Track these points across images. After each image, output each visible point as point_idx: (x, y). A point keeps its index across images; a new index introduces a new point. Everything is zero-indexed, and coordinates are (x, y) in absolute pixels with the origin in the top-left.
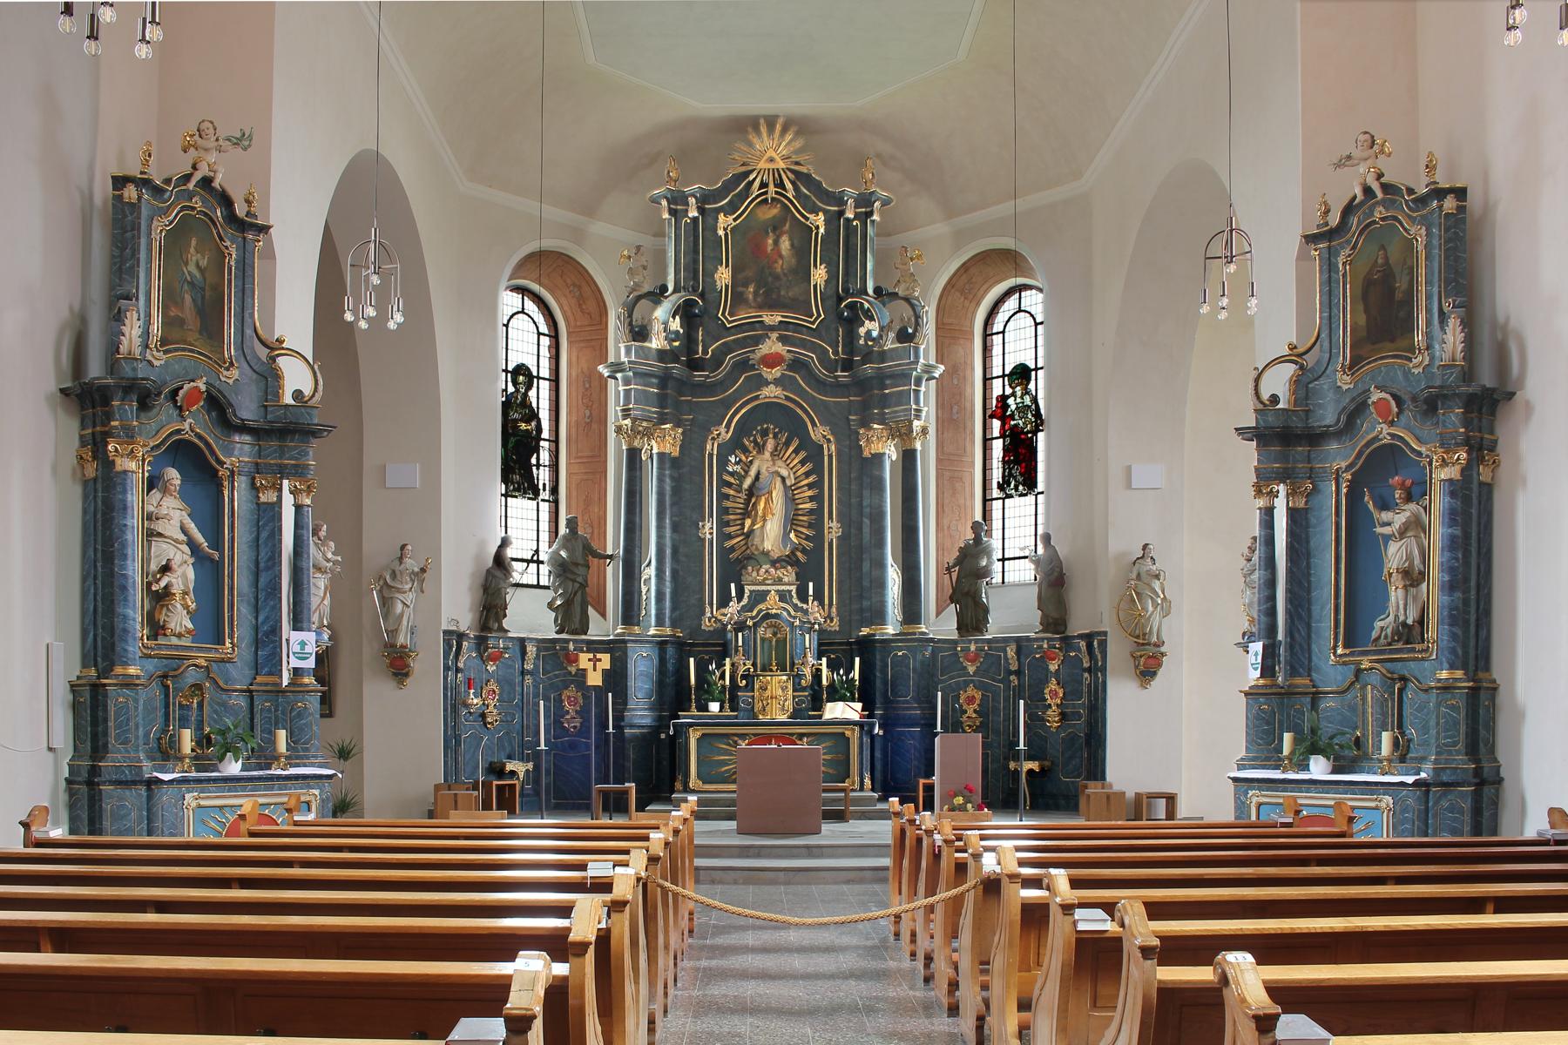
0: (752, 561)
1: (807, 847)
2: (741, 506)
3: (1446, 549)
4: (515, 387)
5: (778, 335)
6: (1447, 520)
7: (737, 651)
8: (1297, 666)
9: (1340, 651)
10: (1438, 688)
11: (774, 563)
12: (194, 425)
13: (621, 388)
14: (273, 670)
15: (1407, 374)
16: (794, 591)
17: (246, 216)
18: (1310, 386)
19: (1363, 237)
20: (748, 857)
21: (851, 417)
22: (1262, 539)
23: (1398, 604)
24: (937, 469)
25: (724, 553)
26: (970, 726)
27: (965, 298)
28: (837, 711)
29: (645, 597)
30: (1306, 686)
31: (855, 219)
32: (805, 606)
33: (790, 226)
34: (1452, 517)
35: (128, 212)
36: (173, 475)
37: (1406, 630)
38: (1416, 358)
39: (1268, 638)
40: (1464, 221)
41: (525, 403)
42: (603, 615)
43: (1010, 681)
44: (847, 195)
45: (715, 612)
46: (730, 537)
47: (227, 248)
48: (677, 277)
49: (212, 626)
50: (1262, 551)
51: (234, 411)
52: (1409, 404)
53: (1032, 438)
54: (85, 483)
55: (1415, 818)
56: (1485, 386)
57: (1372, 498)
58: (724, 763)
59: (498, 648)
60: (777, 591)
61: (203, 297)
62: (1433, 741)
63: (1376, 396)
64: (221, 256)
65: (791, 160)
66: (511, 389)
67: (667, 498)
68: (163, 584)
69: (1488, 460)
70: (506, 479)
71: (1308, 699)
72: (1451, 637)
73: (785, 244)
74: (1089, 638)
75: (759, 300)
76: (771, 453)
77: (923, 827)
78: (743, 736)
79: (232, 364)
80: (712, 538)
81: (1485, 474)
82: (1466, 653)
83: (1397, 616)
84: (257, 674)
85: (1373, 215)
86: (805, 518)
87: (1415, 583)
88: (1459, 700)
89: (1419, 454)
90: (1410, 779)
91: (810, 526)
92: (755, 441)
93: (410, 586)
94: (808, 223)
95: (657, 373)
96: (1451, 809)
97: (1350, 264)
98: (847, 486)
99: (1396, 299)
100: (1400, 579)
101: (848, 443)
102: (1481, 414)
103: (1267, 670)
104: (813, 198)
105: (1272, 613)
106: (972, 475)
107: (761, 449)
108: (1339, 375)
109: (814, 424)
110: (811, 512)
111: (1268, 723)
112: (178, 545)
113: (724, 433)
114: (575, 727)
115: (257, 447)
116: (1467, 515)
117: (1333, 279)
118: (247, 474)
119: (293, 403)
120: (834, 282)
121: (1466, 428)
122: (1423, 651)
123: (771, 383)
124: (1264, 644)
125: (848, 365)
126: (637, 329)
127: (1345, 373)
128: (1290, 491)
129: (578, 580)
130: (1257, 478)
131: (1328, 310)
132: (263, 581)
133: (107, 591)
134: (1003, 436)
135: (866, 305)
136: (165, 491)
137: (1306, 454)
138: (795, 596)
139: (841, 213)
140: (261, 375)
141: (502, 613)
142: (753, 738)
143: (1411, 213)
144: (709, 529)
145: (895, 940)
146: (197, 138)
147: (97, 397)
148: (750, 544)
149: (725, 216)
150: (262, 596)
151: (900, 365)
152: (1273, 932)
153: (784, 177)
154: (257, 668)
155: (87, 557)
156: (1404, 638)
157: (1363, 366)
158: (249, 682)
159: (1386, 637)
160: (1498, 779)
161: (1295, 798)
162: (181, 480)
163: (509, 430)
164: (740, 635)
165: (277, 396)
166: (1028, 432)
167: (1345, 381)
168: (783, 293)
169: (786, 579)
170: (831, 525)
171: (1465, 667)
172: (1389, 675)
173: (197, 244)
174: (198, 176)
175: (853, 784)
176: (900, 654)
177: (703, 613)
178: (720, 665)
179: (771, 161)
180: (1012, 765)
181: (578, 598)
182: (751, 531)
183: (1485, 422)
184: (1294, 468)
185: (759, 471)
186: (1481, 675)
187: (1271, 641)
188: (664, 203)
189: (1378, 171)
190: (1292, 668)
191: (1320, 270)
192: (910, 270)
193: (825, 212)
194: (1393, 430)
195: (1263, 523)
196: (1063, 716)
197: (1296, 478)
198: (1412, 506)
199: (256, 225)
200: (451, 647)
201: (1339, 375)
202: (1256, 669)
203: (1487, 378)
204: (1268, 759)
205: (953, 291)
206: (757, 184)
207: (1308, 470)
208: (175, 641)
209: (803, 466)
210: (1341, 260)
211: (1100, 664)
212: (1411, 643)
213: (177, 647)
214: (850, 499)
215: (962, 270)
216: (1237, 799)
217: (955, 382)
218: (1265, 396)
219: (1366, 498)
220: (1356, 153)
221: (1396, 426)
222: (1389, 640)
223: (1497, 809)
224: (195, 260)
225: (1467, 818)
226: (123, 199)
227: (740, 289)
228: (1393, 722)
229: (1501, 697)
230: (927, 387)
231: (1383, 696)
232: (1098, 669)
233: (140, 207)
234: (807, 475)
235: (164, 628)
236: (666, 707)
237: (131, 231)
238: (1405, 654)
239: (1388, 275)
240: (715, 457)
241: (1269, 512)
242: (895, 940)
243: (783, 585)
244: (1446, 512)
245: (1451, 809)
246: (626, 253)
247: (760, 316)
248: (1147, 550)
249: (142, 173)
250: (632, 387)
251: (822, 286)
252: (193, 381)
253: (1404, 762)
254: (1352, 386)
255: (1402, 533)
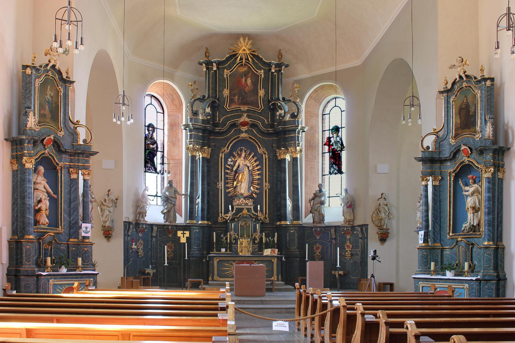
0: (237, 197)
1: (261, 301)
2: (232, 177)
3: (487, 201)
4: (149, 132)
5: (246, 115)
6: (487, 191)
7: (231, 230)
8: (436, 239)
9: (451, 234)
10: (484, 248)
11: (245, 198)
12: (49, 151)
13: (189, 133)
14: (76, 237)
15: (474, 140)
16: (252, 208)
17: (66, 78)
18: (441, 143)
19: (459, 93)
20: (240, 304)
21: (274, 145)
22: (424, 196)
23: (471, 219)
24: (305, 164)
25: (226, 194)
26: (318, 258)
27: (316, 102)
28: (267, 252)
29: (197, 210)
30: (439, 246)
31: (275, 72)
32: (256, 214)
33: (251, 75)
34: (489, 190)
35: (27, 77)
36: (41, 169)
37: (474, 228)
38: (477, 135)
39: (426, 230)
40: (493, 89)
41: (152, 138)
42: (181, 216)
43: (332, 242)
44: (272, 63)
45: (223, 215)
46: (228, 188)
47: (60, 89)
48: (209, 92)
49: (54, 222)
50: (424, 200)
51: (63, 147)
52: (474, 151)
53: (340, 153)
54: (13, 171)
55: (476, 291)
56: (500, 146)
57: (462, 182)
58: (227, 271)
59: (143, 228)
60: (246, 208)
61: (52, 107)
62: (482, 265)
63: (463, 147)
64: (58, 92)
65: (251, 50)
66: (147, 132)
67: (206, 174)
68: (39, 206)
69: (501, 171)
70: (145, 166)
71: (440, 251)
72: (488, 231)
73: (249, 81)
74: (361, 226)
75: (239, 101)
76: (244, 158)
77: (310, 293)
78: (234, 261)
79: (61, 130)
80: (222, 188)
81: (500, 175)
82: (493, 236)
83: (470, 223)
84: (70, 238)
85: (462, 85)
86: (256, 182)
87: (477, 211)
88: (491, 252)
89: (478, 168)
90: (474, 278)
91: (258, 184)
92: (238, 153)
93: (111, 205)
94: (257, 73)
95: (202, 128)
96: (488, 289)
97: (454, 102)
98: (272, 170)
99: (470, 114)
100: (471, 210)
101: (272, 154)
102: (499, 155)
103: (425, 241)
104: (259, 64)
105: (427, 221)
106: (318, 167)
107: (240, 156)
108: (450, 140)
109: (260, 147)
110: (259, 179)
111: (426, 259)
112: (43, 193)
113: (226, 150)
114: (171, 257)
115: (70, 159)
116: (494, 189)
117: (448, 107)
118: (67, 168)
119: (83, 144)
120: (267, 96)
121: (493, 160)
122: (479, 235)
123: (244, 132)
124: (424, 232)
125: (272, 126)
126: (194, 112)
127: (453, 139)
128: (433, 179)
129: (173, 203)
130: (422, 174)
131: (447, 117)
132: (72, 206)
133: (21, 209)
134: (329, 152)
135: (279, 104)
136: (38, 174)
137: (439, 166)
138: (253, 210)
139: (270, 70)
140: (72, 134)
141: (144, 215)
142: (238, 262)
143: (475, 85)
144: (221, 185)
145: (298, 331)
146: (50, 51)
147: (18, 142)
148: (236, 191)
149: (226, 70)
150: (72, 211)
151: (292, 127)
152: (423, 322)
153: (249, 56)
154: (70, 236)
155: (14, 197)
156: (473, 230)
157: (459, 137)
158: (67, 240)
159: (467, 230)
160: (505, 278)
161: (435, 285)
162: (44, 170)
163: (147, 148)
164: (233, 224)
165: (77, 141)
166: (338, 151)
167: (452, 141)
168: (248, 99)
169: (249, 204)
170: (266, 184)
171: (493, 241)
172: (468, 243)
173: (50, 88)
174: (51, 65)
175: (275, 278)
176: (292, 231)
177: (219, 216)
178: (225, 235)
179: (244, 50)
180: (333, 272)
181: (173, 210)
182: (236, 186)
183: (500, 158)
184: (435, 171)
185: (239, 164)
186: (499, 243)
187: (427, 231)
188: (204, 65)
189: (464, 71)
190: (434, 240)
191: (444, 103)
192: (295, 92)
193: (264, 70)
194: (469, 159)
195: (424, 190)
196: (352, 255)
197: (436, 175)
198: (476, 185)
199: (70, 81)
200: (126, 227)
201: (450, 140)
202: (421, 240)
203: (501, 144)
204: (426, 271)
205: (311, 99)
206: (239, 57)
207: (440, 172)
208: (42, 226)
209: (255, 162)
210: (451, 100)
211: (365, 236)
212: (475, 232)
213: (43, 229)
214: (273, 175)
215: (315, 92)
216: (415, 285)
217: (312, 132)
218: (425, 146)
219: (460, 182)
220: (457, 64)
221: (470, 158)
222: (468, 231)
223: (505, 289)
224: (50, 93)
225: (494, 292)
226: (26, 73)
227: (232, 97)
228: (469, 259)
229: (506, 251)
230: (302, 135)
231: (466, 250)
232: (364, 238)
233: (32, 76)
234: (257, 166)
235: (39, 222)
236: (205, 250)
237: (29, 84)
238: (473, 236)
239: (467, 106)
240: (223, 159)
241: (426, 186)
242: (298, 331)
243: (249, 206)
244: (487, 188)
245: (488, 289)
246: (190, 84)
247: (240, 107)
248: (383, 195)
249: (32, 64)
250: (193, 133)
251: (263, 97)
252: (49, 136)
253: (473, 273)
254: (455, 144)
255: (472, 194)
